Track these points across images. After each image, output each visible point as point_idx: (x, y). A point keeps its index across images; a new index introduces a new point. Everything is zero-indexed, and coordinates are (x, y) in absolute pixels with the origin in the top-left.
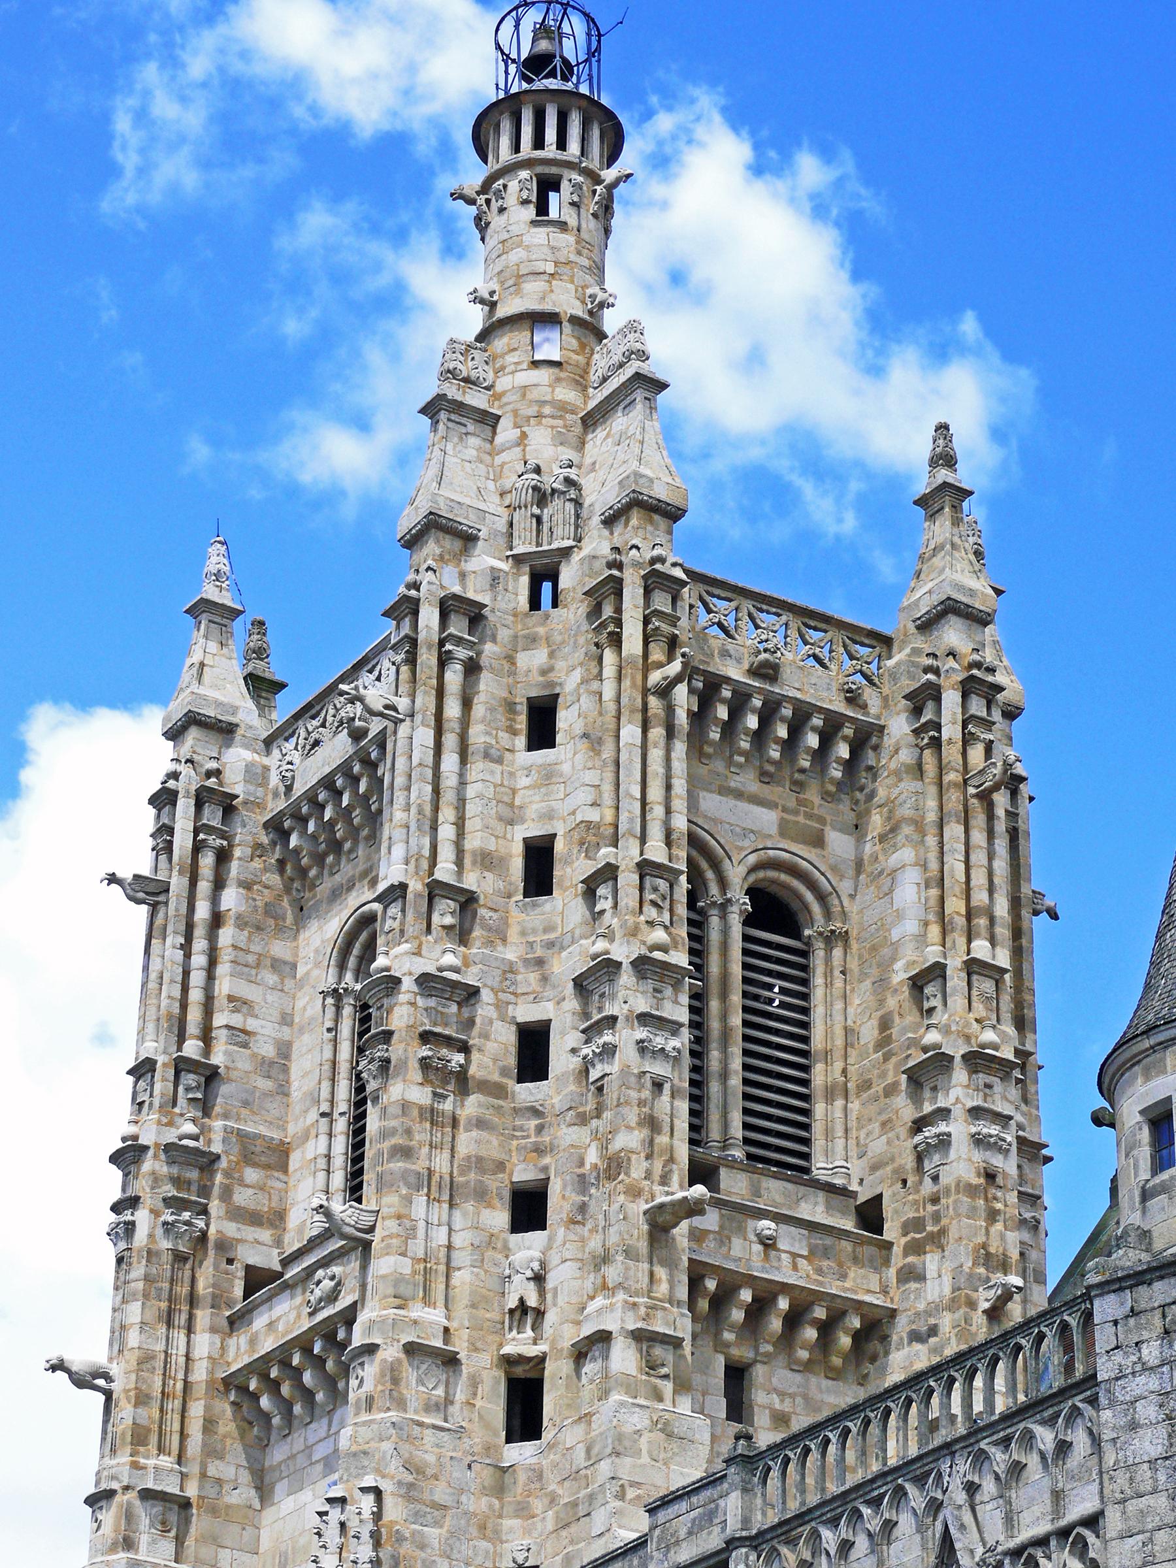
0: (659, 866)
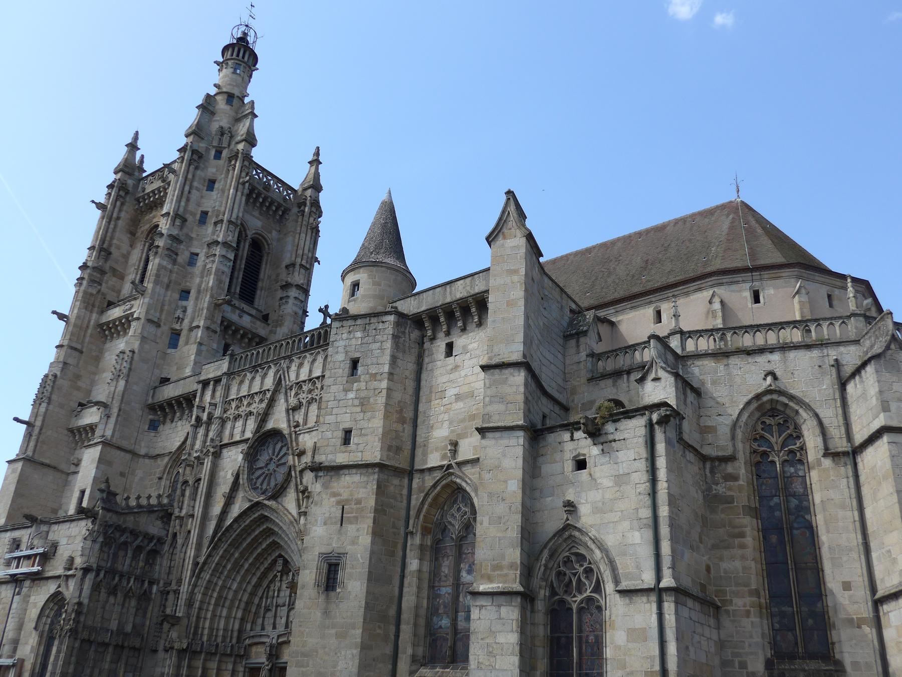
0: (233, 222)
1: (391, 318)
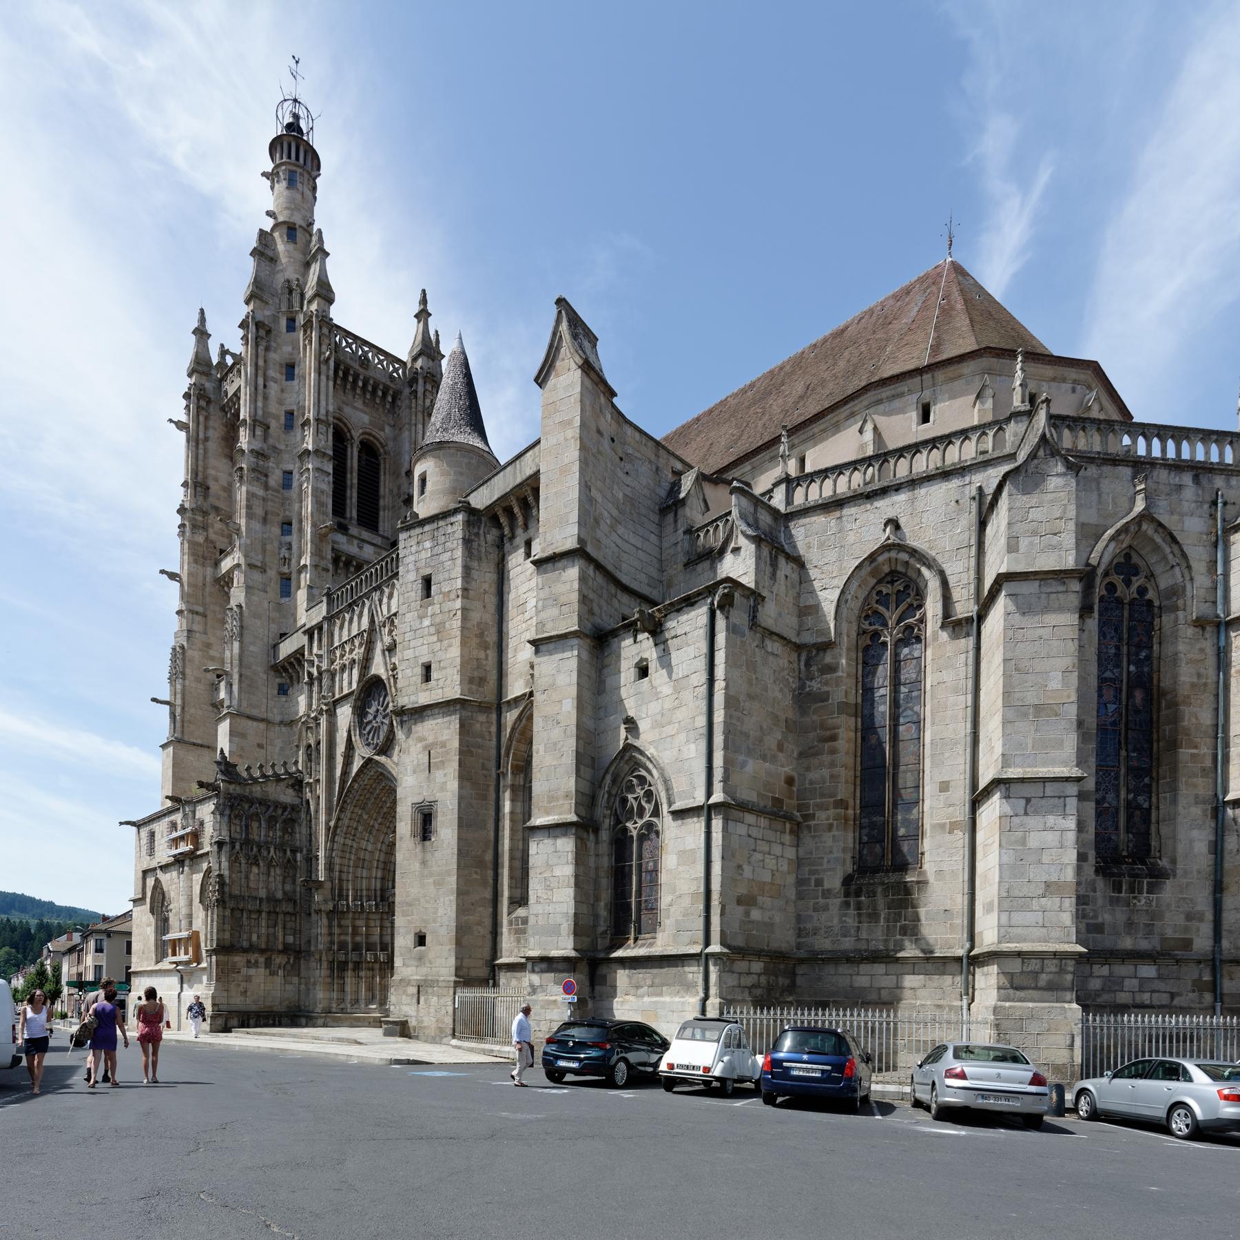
0: (323, 421)
1: (460, 517)
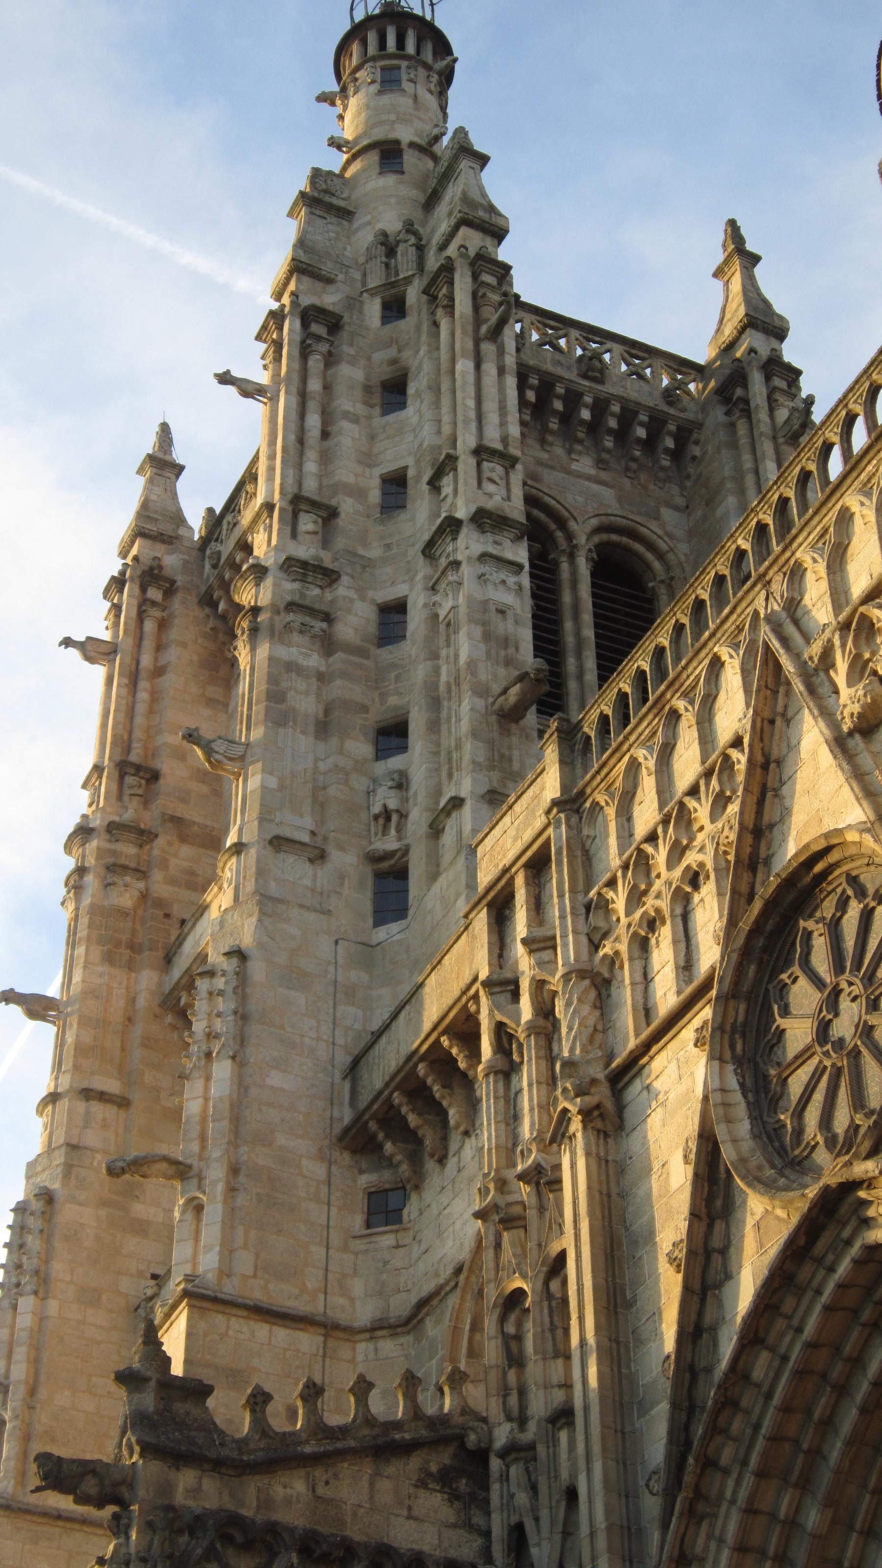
0: (493, 452)
